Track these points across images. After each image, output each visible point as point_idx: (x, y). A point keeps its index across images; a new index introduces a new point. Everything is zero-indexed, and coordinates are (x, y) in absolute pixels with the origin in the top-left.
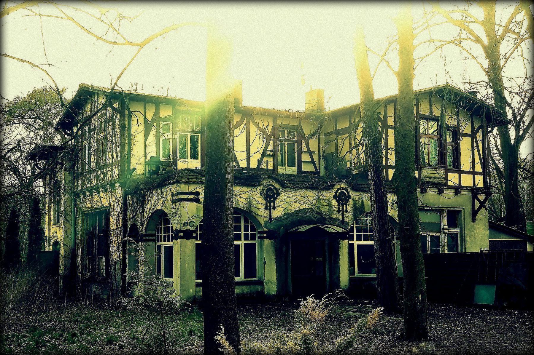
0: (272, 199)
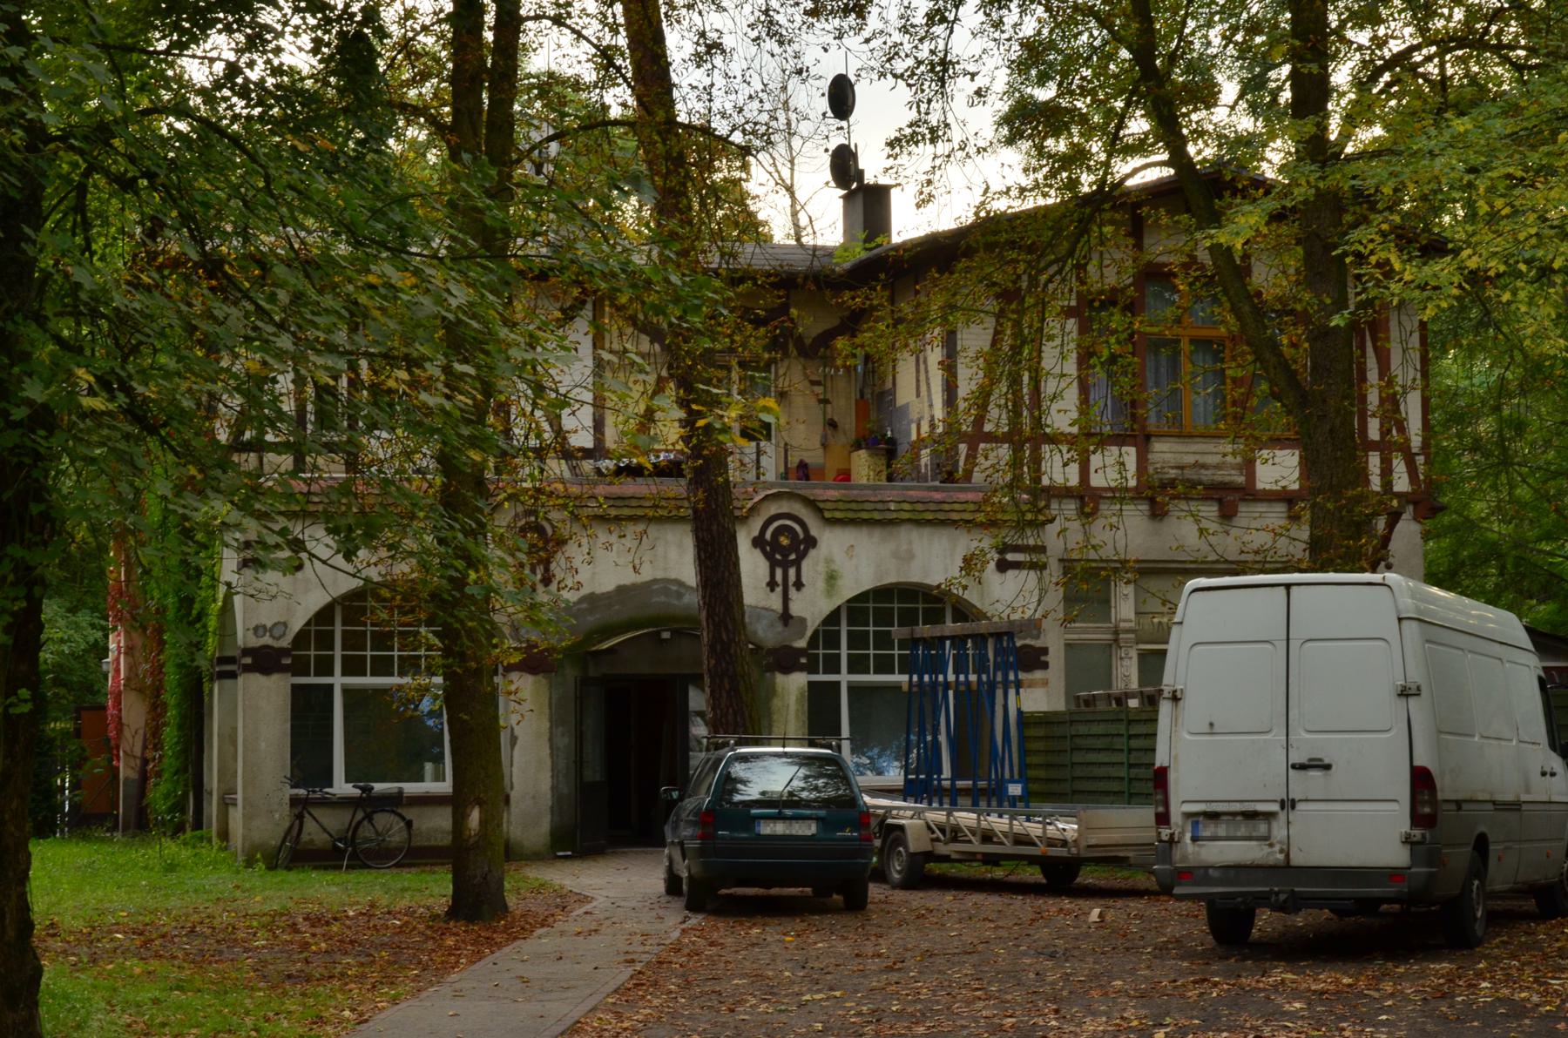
0: (793, 557)
